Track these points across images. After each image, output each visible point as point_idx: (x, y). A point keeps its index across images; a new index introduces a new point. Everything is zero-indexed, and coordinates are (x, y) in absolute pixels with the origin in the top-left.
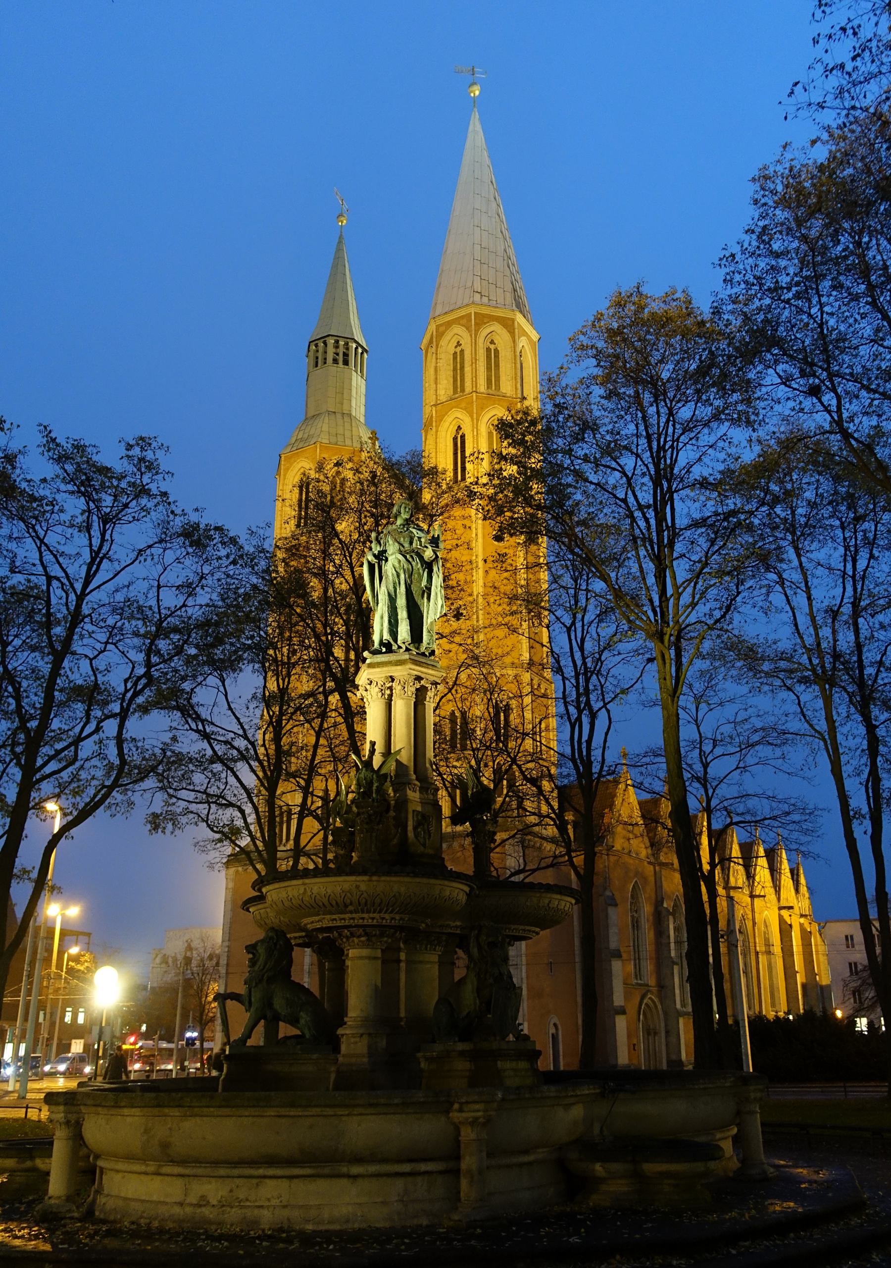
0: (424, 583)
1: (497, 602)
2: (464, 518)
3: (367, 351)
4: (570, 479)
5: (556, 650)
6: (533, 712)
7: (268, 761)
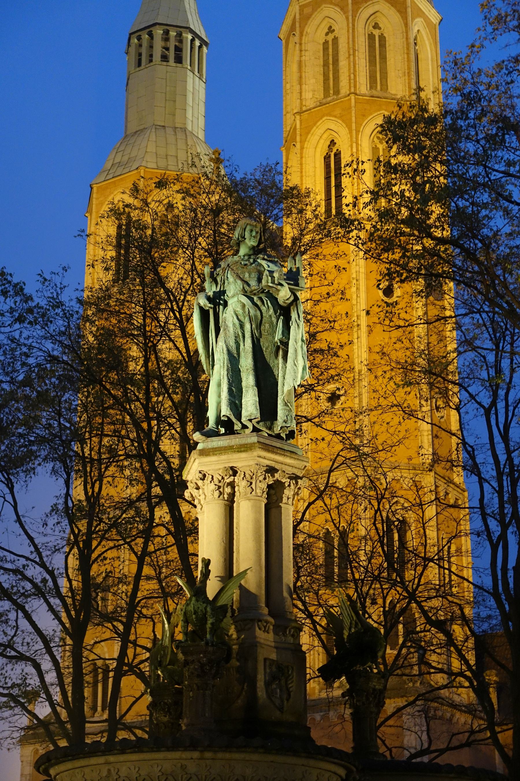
0: (278, 336)
1: (388, 375)
2: (337, 256)
3: (206, 44)
4: (485, 197)
5: (470, 440)
6: (438, 530)
7: (73, 597)
